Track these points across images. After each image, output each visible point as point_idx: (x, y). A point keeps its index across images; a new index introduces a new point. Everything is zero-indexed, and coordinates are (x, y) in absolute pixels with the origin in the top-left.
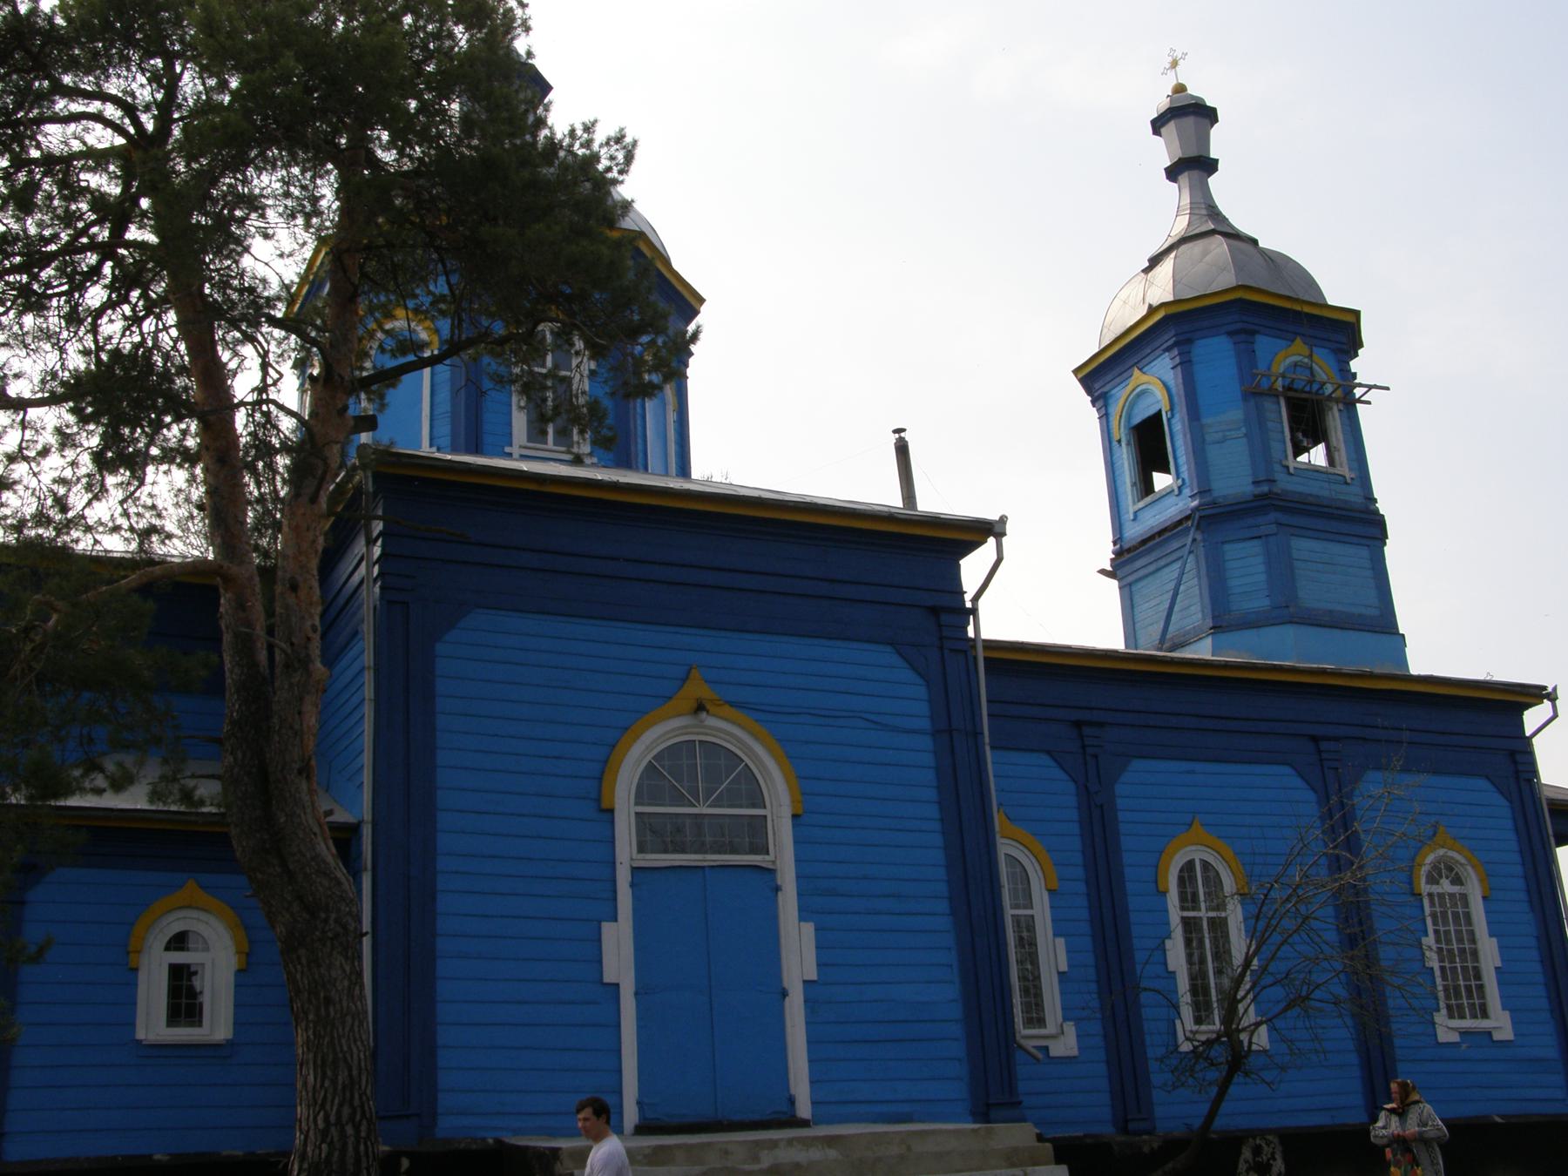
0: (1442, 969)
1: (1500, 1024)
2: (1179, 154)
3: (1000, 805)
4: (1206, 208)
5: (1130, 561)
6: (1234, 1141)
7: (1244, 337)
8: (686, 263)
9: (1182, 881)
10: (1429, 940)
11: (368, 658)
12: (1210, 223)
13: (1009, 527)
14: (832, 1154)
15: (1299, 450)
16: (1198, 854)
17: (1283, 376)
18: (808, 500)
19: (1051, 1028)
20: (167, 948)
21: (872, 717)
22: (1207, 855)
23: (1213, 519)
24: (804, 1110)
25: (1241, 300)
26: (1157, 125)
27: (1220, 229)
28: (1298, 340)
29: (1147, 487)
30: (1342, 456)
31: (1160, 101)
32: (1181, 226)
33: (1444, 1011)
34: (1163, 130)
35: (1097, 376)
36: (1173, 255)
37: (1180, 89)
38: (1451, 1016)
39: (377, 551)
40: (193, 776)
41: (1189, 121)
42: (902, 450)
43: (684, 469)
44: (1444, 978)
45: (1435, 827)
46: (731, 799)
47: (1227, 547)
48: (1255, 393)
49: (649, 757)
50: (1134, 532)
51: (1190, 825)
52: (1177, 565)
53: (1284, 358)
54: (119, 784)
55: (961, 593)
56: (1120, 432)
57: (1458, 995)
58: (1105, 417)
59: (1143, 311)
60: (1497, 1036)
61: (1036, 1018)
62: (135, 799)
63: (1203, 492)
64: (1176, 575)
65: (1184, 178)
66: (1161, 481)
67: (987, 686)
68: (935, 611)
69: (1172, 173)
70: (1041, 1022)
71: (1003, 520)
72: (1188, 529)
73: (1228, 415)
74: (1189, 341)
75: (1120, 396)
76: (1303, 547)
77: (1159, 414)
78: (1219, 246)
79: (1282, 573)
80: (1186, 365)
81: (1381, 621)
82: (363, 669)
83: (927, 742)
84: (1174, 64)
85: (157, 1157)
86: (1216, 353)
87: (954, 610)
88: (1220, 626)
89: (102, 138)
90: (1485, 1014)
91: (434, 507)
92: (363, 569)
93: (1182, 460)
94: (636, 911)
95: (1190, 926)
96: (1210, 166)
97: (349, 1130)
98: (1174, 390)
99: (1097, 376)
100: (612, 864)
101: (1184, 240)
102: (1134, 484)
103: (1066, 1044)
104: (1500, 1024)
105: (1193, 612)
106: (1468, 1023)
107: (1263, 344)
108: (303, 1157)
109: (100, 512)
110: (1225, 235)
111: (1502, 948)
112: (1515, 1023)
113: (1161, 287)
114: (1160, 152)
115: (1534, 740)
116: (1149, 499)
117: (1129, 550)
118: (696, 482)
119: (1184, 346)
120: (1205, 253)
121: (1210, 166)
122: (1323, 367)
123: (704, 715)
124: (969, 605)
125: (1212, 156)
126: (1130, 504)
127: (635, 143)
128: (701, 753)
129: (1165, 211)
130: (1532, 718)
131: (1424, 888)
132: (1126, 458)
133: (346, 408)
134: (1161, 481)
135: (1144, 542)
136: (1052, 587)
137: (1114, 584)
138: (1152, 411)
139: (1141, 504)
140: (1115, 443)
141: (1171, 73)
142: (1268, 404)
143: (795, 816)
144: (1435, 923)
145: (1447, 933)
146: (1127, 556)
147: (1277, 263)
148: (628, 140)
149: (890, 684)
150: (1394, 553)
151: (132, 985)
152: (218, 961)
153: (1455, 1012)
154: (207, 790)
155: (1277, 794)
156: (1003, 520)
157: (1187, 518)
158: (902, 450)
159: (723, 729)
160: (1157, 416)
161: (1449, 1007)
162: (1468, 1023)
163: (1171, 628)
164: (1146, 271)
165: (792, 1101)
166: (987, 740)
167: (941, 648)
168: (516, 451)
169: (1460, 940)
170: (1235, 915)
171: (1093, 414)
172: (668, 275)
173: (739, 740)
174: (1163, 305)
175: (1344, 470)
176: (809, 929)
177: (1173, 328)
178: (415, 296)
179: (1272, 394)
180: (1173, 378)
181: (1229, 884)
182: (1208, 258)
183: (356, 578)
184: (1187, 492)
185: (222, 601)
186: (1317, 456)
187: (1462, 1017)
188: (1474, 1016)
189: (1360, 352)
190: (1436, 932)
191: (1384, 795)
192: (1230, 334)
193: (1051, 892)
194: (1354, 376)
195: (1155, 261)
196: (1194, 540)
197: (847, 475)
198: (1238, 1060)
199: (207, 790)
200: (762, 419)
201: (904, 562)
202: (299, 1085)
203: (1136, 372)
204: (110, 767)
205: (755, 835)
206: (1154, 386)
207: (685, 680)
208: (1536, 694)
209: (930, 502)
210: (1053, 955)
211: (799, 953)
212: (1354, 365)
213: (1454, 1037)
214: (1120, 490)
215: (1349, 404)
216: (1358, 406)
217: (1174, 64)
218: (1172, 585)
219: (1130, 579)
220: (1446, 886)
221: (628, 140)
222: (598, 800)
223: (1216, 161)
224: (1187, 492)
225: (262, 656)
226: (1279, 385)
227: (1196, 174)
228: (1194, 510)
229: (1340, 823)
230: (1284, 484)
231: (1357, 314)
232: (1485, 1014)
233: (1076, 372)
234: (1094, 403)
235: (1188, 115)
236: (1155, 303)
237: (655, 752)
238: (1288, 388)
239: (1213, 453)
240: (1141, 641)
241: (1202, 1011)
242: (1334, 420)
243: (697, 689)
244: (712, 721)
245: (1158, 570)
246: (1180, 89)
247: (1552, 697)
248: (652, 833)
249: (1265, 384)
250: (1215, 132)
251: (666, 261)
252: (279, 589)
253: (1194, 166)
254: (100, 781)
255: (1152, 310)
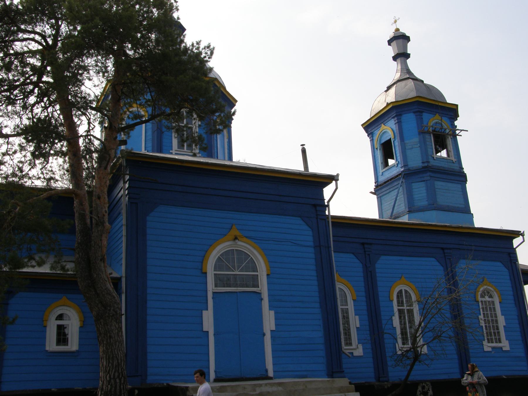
0: (486, 326)
1: (505, 345)
2: (397, 52)
3: (337, 271)
4: (406, 70)
5: (380, 189)
6: (416, 384)
7: (419, 113)
8: (231, 88)
9: (398, 297)
10: (481, 317)
11: (124, 222)
12: (407, 75)
13: (340, 178)
14: (280, 388)
15: (437, 151)
16: (403, 288)
17: (432, 127)
18: (272, 168)
19: (354, 346)
20: (56, 319)
21: (294, 241)
22: (406, 288)
23: (409, 175)
24: (271, 374)
25: (418, 101)
26: (390, 42)
27: (411, 77)
28: (437, 115)
29: (386, 164)
30: (452, 153)
31: (391, 34)
32: (398, 76)
33: (486, 341)
34: (392, 44)
35: (370, 127)
36: (395, 86)
37: (397, 30)
38: (489, 342)
39: (127, 186)
40: (65, 261)
41: (401, 41)
42: (304, 151)
43: (230, 158)
44: (486, 329)
45: (483, 278)
46: (246, 269)
47: (413, 184)
48: (422, 132)
49: (219, 255)
50: (382, 179)
51: (401, 278)
52: (396, 190)
53: (432, 120)
54: (40, 264)
55: (324, 200)
56: (377, 146)
57: (491, 335)
58: (372, 140)
59: (385, 105)
60: (504, 349)
61: (349, 343)
62: (45, 269)
63: (405, 166)
64: (396, 193)
65: (399, 60)
66: (391, 162)
67: (332, 231)
68: (315, 206)
69: (395, 58)
70: (350, 344)
71: (338, 175)
72: (400, 178)
73: (414, 140)
74: (401, 115)
75: (377, 133)
76: (439, 184)
77: (390, 139)
78: (411, 83)
79: (432, 193)
80: (399, 123)
81: (465, 209)
82: (122, 225)
83: (312, 250)
84: (395, 22)
85: (53, 390)
86: (409, 119)
87: (321, 206)
88: (411, 211)
89: (34, 46)
90: (500, 342)
91: (146, 171)
92: (122, 192)
93: (398, 155)
94: (214, 307)
95: (401, 312)
96: (408, 56)
97: (118, 381)
98: (395, 131)
99: (370, 127)
100: (206, 291)
101: (399, 81)
102: (382, 163)
103: (359, 352)
104: (505, 345)
105: (402, 206)
106: (494, 345)
107: (425, 116)
108: (102, 390)
109: (34, 172)
110: (413, 79)
111: (506, 319)
112: (510, 344)
113: (391, 97)
114: (391, 51)
115: (517, 249)
116: (387, 168)
117: (380, 185)
118: (235, 162)
119: (399, 116)
120: (406, 85)
121: (408, 56)
122: (446, 124)
123: (237, 241)
124: (326, 204)
125: (408, 52)
126: (380, 170)
127: (214, 48)
128: (236, 253)
129: (392, 71)
130: (516, 242)
131: (480, 299)
132: (379, 154)
133: (116, 137)
134: (391, 162)
135: (385, 182)
136: (354, 198)
137: (375, 197)
138: (388, 138)
139: (384, 170)
140: (375, 149)
141: (394, 25)
142: (427, 136)
143: (268, 275)
144: (483, 311)
145: (487, 314)
146: (379, 187)
147: (430, 89)
148: (212, 47)
149: (300, 230)
150: (470, 186)
151: (45, 332)
152: (73, 324)
153: (490, 341)
154: (70, 266)
155: (430, 267)
156: (338, 175)
157: (400, 174)
158: (304, 151)
159: (244, 246)
160: (390, 140)
161: (488, 339)
162: (494, 345)
163: (394, 212)
164: (386, 91)
165: (267, 371)
166: (332, 249)
167: (317, 218)
168: (174, 152)
169: (492, 317)
170: (416, 308)
171: (368, 139)
172: (225, 93)
173: (249, 249)
174: (392, 103)
175: (453, 158)
176: (272, 313)
177: (395, 110)
178: (140, 100)
179: (428, 133)
180: (395, 127)
181: (414, 298)
182: (407, 87)
183: (120, 195)
184: (400, 166)
185: (75, 202)
186: (443, 153)
187: (492, 342)
188: (496, 342)
189: (458, 118)
190: (484, 314)
191: (466, 268)
192: (414, 112)
193: (354, 300)
194: (456, 126)
195: (389, 88)
196: (402, 182)
197: (285, 160)
198: (417, 357)
199: (70, 266)
200: (256, 141)
201: (304, 189)
202: (101, 365)
203: (383, 125)
204: (37, 258)
205: (254, 281)
206: (389, 130)
207: (230, 229)
208: (517, 234)
209: (313, 169)
210: (355, 322)
211: (269, 321)
212: (456, 123)
213: (490, 349)
214: (377, 165)
215: (454, 136)
216: (457, 137)
217: (395, 22)
218: (395, 197)
219: (381, 195)
220: (487, 298)
221: (212, 47)
222: (201, 269)
223: (410, 54)
224: (400, 166)
225: (88, 221)
226: (431, 130)
227: (403, 58)
228: (402, 172)
229: (451, 277)
230: (432, 163)
231: (457, 106)
232: (500, 342)
233: (362, 125)
234: (368, 136)
235: (400, 39)
236: (389, 102)
237: (221, 253)
238: (434, 131)
239: (408, 152)
240: (384, 216)
241: (405, 340)
242: (449, 141)
243: (235, 232)
244: (240, 243)
245: (390, 192)
246: (397, 30)
247: (523, 235)
248: (220, 281)
249: (426, 129)
250: (409, 44)
251: (224, 88)
252: (94, 198)
253: (402, 56)
254: (34, 263)
255: (388, 104)
